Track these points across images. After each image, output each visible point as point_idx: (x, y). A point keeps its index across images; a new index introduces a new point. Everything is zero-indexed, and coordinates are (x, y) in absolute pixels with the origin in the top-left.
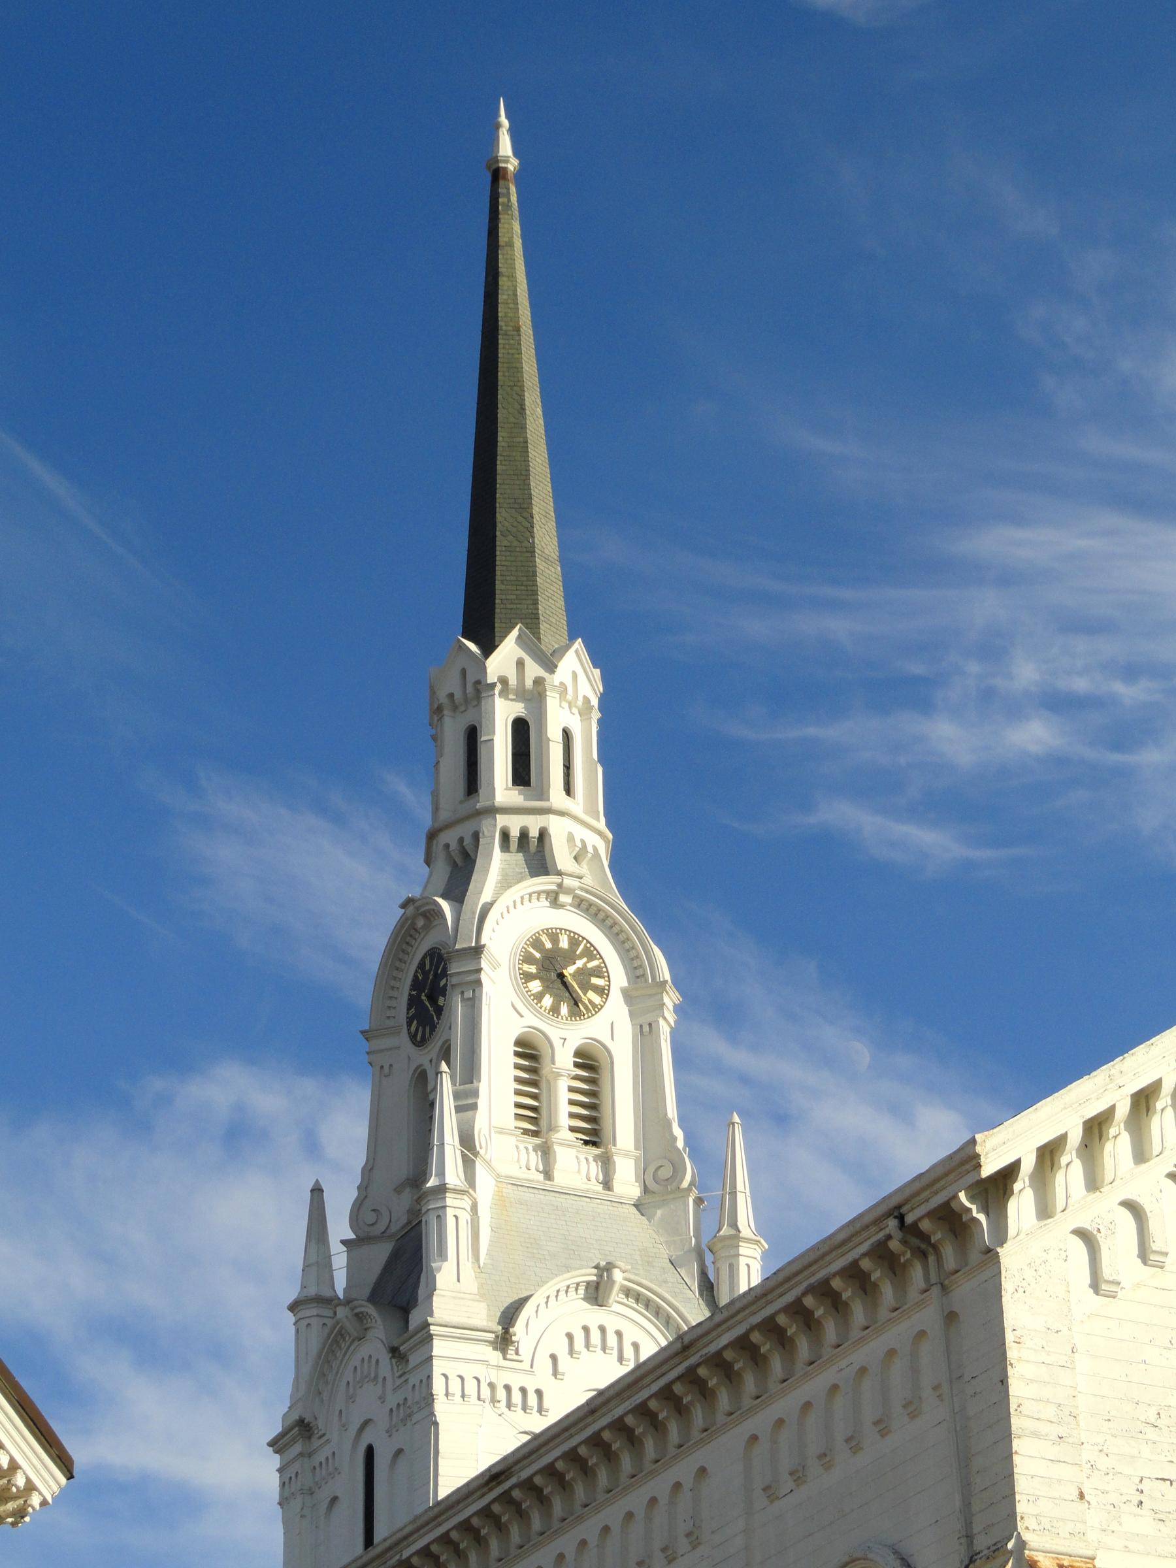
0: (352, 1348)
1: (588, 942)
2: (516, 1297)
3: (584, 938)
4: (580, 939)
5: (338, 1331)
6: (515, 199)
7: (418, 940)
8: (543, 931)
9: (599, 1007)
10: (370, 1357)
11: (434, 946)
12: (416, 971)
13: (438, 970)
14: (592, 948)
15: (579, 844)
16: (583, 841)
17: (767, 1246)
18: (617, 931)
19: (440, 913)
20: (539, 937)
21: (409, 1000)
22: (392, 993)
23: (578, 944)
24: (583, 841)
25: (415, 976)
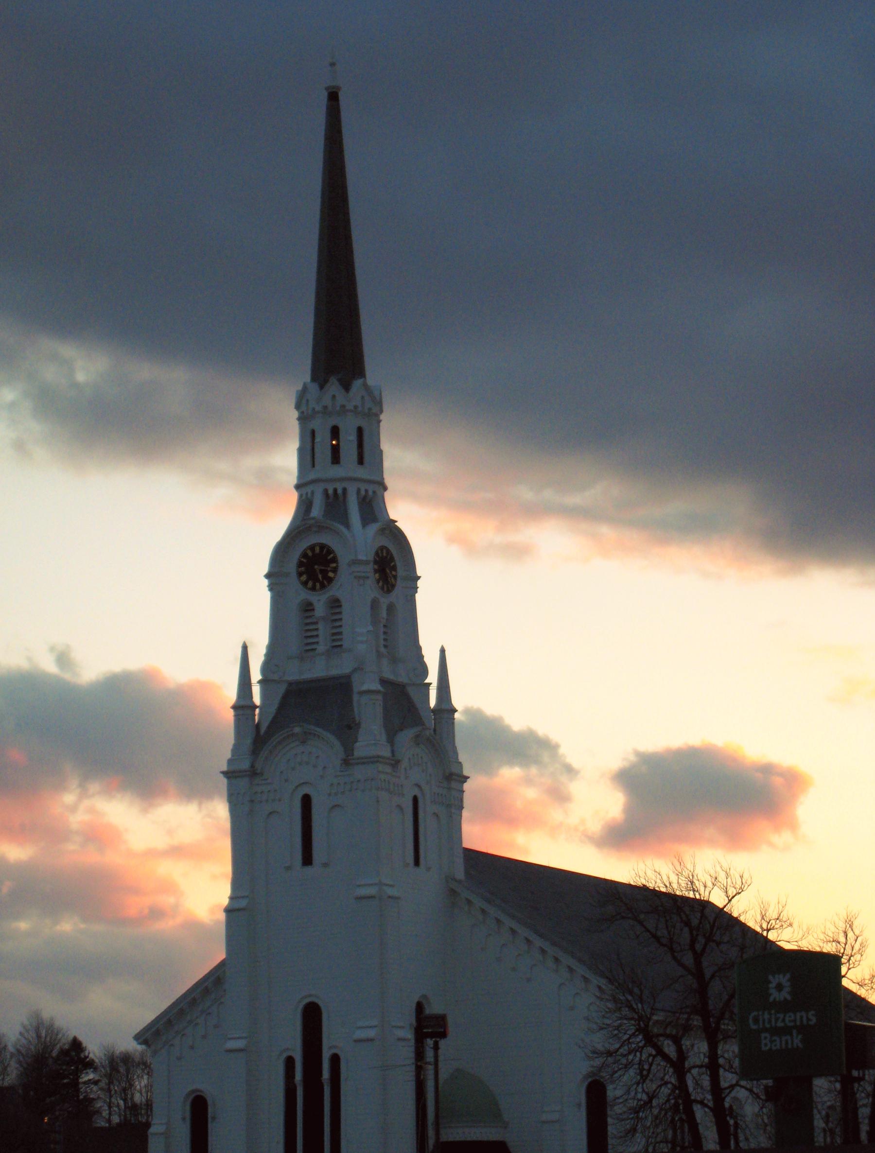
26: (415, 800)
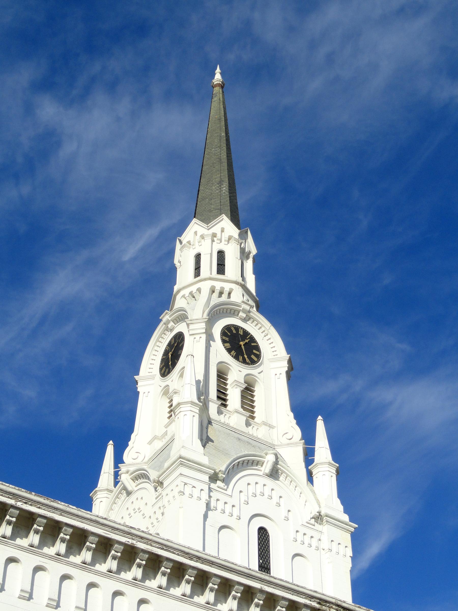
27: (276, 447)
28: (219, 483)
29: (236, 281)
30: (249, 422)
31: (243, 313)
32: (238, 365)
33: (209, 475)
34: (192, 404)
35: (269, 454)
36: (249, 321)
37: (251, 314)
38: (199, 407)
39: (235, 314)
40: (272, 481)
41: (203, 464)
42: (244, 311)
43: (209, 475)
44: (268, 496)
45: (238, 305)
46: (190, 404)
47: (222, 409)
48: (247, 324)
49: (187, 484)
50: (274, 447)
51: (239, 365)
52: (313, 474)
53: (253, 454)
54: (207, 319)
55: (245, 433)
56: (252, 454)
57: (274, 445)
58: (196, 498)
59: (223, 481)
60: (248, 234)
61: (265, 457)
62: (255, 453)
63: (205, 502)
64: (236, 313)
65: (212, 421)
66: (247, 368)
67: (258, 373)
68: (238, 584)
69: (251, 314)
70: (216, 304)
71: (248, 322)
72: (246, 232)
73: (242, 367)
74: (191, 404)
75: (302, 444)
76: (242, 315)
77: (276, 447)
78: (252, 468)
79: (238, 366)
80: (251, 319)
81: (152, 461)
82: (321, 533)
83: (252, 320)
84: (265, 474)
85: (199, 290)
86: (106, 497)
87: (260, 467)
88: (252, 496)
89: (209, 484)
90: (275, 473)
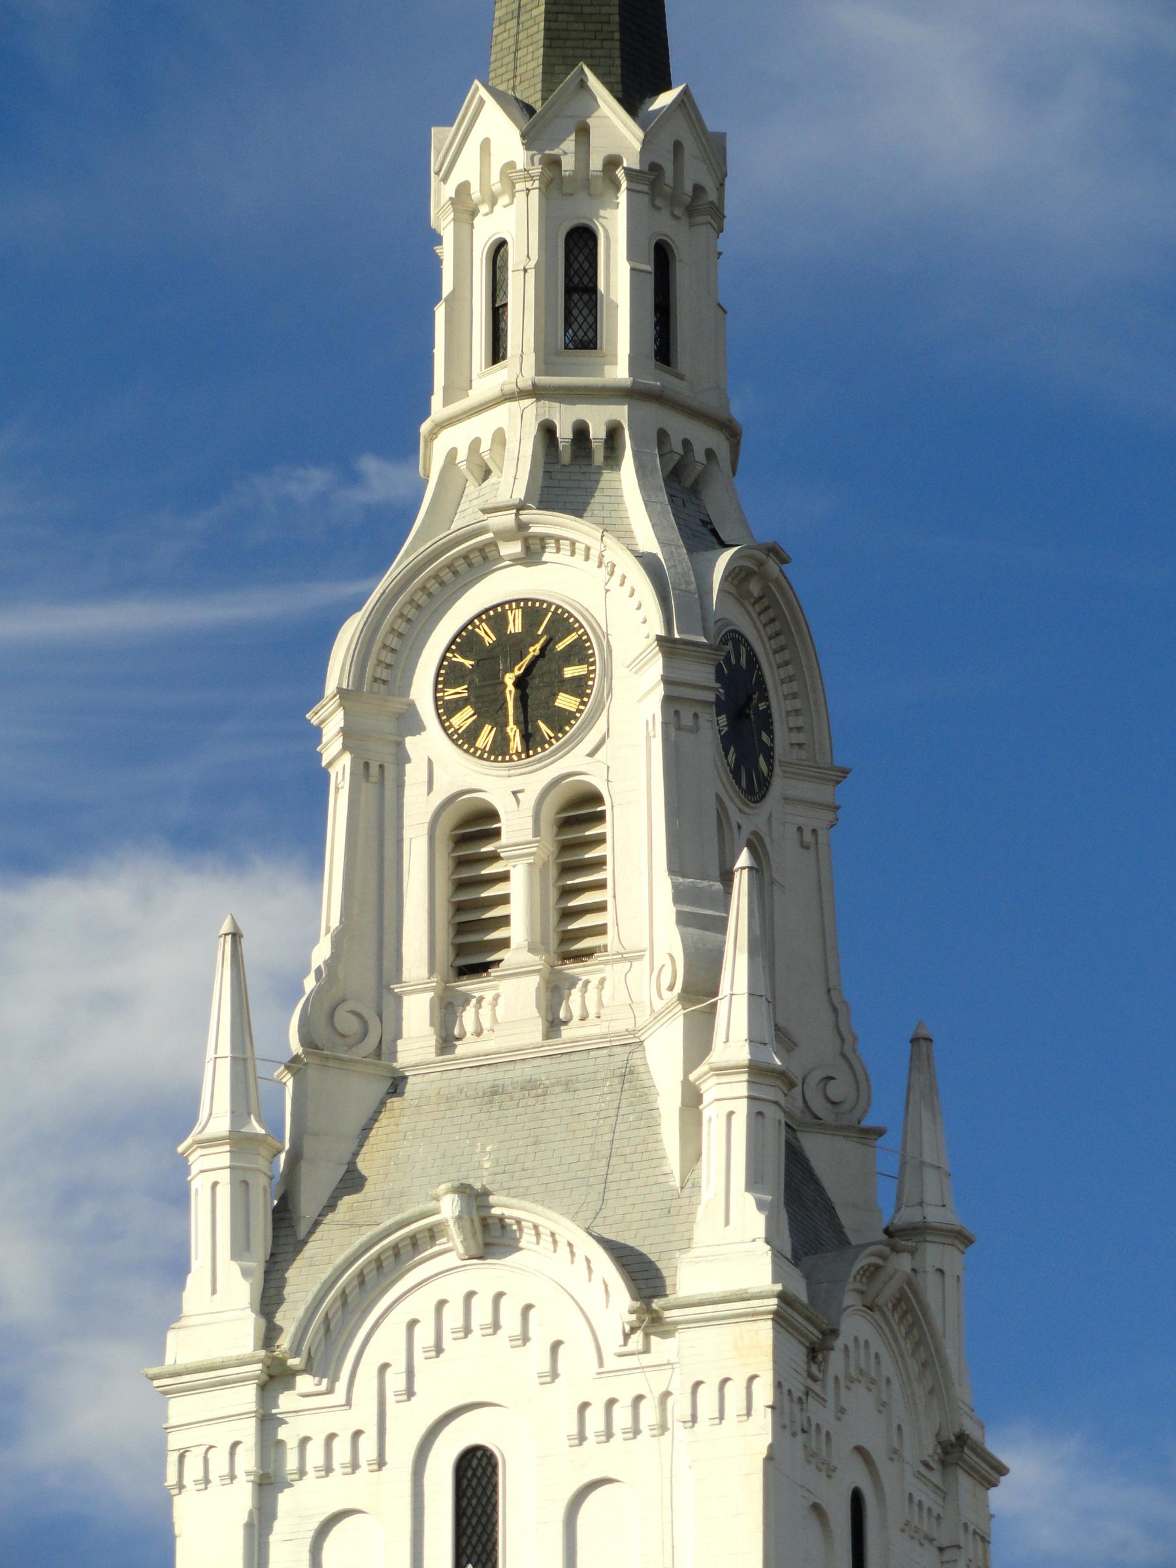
0: (854, 1139)
1: (448, 649)
2: (584, 1259)
3: (444, 658)
4: (445, 663)
5: (915, 1310)
6: (744, 659)
7: (750, 608)
8: (474, 754)
9: (447, 724)
10: (856, 1339)
11: (758, 805)
12: (772, 741)
13: (756, 871)
14: (464, 634)
15: (678, 447)
16: (686, 444)
17: (494, 639)
18: (425, 597)
19: (730, 574)
20: (488, 752)
21: (771, 724)
22: (801, 738)
23: (454, 666)
24: (686, 444)
25: (770, 732)
26: (857, 1501)
27: (642, 1034)
28: (305, 1382)
29: (503, 395)
30: (567, 974)
31: (507, 541)
32: (507, 773)
33: (256, 1381)
34: (202, 1147)
35: (442, 1195)
36: (547, 550)
37: (532, 530)
38: (227, 1144)
39: (490, 559)
40: (496, 1266)
41: (220, 1362)
42: (505, 535)
43: (256, 1381)
44: (481, 1329)
45: (474, 530)
46: (199, 1150)
47: (462, 986)
48: (546, 563)
49: (188, 1449)
50: (638, 1037)
51: (512, 772)
52: (166, 1481)
53: (396, 1223)
54: (338, 696)
55: (523, 1050)
56: (390, 1226)
57: (634, 1034)
58: (219, 1481)
59: (308, 1369)
60: (591, 90)
61: (440, 1208)
62: (398, 1217)
63: (248, 1482)
64: (491, 555)
65: (407, 1074)
66: (543, 763)
67: (587, 755)
68: (879, 1363)
69: (532, 530)
70: (387, 590)
71: (545, 557)
72: (583, 84)
73: (523, 770)
74: (198, 1147)
75: (680, 1007)
76: (512, 548)
77: (642, 1034)
78: (420, 1259)
79: (509, 776)
80: (548, 541)
81: (661, 1026)
82: (670, 1366)
83: (551, 544)
84: (467, 1257)
85: (499, 438)
86: (713, 1099)
87: (444, 1240)
88: (426, 1359)
89: (254, 1415)
90: (499, 1233)
